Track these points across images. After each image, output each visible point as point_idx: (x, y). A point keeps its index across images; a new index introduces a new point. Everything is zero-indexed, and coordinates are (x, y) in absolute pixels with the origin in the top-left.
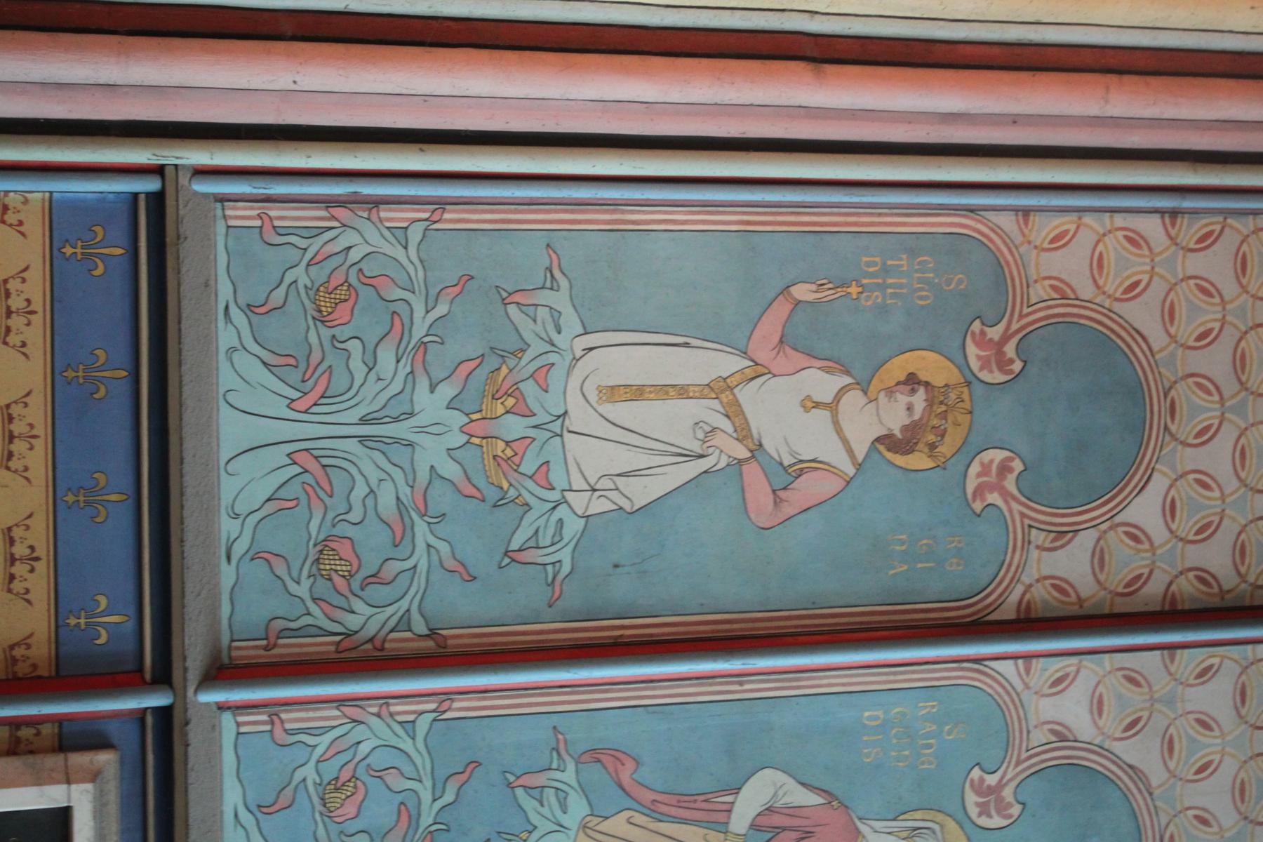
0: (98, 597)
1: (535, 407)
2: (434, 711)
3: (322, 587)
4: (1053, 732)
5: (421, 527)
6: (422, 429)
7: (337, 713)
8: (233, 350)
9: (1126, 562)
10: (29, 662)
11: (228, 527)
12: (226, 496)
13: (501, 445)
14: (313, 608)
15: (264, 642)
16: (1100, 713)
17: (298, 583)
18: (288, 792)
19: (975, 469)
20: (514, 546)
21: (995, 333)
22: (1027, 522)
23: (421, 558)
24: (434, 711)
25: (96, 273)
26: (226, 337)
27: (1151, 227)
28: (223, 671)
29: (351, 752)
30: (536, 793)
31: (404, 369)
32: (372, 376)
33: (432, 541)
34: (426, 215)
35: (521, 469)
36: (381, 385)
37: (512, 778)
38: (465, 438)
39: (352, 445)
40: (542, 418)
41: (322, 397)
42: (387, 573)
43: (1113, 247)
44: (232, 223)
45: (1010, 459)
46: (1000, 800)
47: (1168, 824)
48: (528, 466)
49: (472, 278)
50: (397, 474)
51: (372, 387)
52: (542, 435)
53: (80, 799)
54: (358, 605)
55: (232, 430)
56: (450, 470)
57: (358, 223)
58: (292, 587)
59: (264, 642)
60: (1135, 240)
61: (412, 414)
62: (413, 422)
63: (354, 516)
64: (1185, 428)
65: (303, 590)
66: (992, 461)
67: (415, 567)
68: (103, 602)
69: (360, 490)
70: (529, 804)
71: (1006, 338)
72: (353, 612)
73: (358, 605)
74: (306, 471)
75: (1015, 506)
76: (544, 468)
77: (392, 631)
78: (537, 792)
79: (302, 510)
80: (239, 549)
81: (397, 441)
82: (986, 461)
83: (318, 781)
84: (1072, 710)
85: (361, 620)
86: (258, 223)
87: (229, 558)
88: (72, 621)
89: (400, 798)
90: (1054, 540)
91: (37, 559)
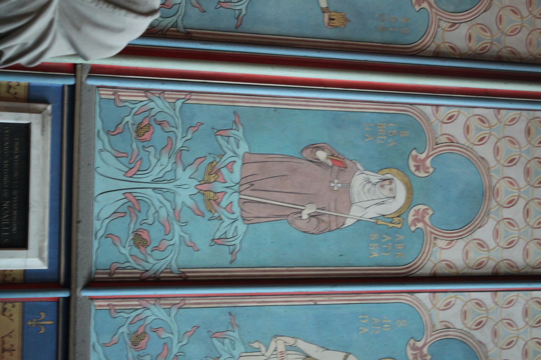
1: (228, 180)
2: (183, 99)
4: (449, 139)
5: (177, 227)
6: (179, 186)
8: (101, 151)
9: (476, 256)
10: (12, 277)
11: (97, 224)
12: (96, 211)
14: (131, 260)
15: (109, 271)
16: (465, 318)
17: (124, 247)
18: (121, 126)
19: (412, 212)
20: (217, 236)
21: (423, 156)
22: (439, 17)
23: (176, 239)
24: (183, 99)
25: (42, 332)
26: (99, 145)
27: (489, 114)
28: (93, 283)
29: (148, 112)
31: (173, 160)
32: (159, 164)
33: (182, 234)
34: (183, 97)
36: (163, 167)
38: (197, 191)
39: (150, 192)
41: (139, 171)
42: (162, 247)
43: (474, 123)
44: (103, 97)
47: (496, 184)
48: (224, 203)
49: (198, 327)
50: (168, 204)
51: (158, 169)
52: (229, 191)
53: (32, 119)
57: (152, 307)
59: (109, 271)
60: (482, 120)
61: (175, 180)
62: (175, 183)
63: (150, 221)
64: (503, 199)
65: (125, 251)
66: (419, 209)
69: (152, 210)
71: (425, 224)
72: (147, 262)
73: (150, 260)
76: (230, 205)
78: (222, 339)
79: (127, 218)
80: (100, 234)
81: (168, 190)
84: (453, 317)
85: (151, 265)
86: (113, 97)
87: (96, 237)
88: (30, 323)
89: (163, 341)
90: (450, 27)
91: (13, 350)
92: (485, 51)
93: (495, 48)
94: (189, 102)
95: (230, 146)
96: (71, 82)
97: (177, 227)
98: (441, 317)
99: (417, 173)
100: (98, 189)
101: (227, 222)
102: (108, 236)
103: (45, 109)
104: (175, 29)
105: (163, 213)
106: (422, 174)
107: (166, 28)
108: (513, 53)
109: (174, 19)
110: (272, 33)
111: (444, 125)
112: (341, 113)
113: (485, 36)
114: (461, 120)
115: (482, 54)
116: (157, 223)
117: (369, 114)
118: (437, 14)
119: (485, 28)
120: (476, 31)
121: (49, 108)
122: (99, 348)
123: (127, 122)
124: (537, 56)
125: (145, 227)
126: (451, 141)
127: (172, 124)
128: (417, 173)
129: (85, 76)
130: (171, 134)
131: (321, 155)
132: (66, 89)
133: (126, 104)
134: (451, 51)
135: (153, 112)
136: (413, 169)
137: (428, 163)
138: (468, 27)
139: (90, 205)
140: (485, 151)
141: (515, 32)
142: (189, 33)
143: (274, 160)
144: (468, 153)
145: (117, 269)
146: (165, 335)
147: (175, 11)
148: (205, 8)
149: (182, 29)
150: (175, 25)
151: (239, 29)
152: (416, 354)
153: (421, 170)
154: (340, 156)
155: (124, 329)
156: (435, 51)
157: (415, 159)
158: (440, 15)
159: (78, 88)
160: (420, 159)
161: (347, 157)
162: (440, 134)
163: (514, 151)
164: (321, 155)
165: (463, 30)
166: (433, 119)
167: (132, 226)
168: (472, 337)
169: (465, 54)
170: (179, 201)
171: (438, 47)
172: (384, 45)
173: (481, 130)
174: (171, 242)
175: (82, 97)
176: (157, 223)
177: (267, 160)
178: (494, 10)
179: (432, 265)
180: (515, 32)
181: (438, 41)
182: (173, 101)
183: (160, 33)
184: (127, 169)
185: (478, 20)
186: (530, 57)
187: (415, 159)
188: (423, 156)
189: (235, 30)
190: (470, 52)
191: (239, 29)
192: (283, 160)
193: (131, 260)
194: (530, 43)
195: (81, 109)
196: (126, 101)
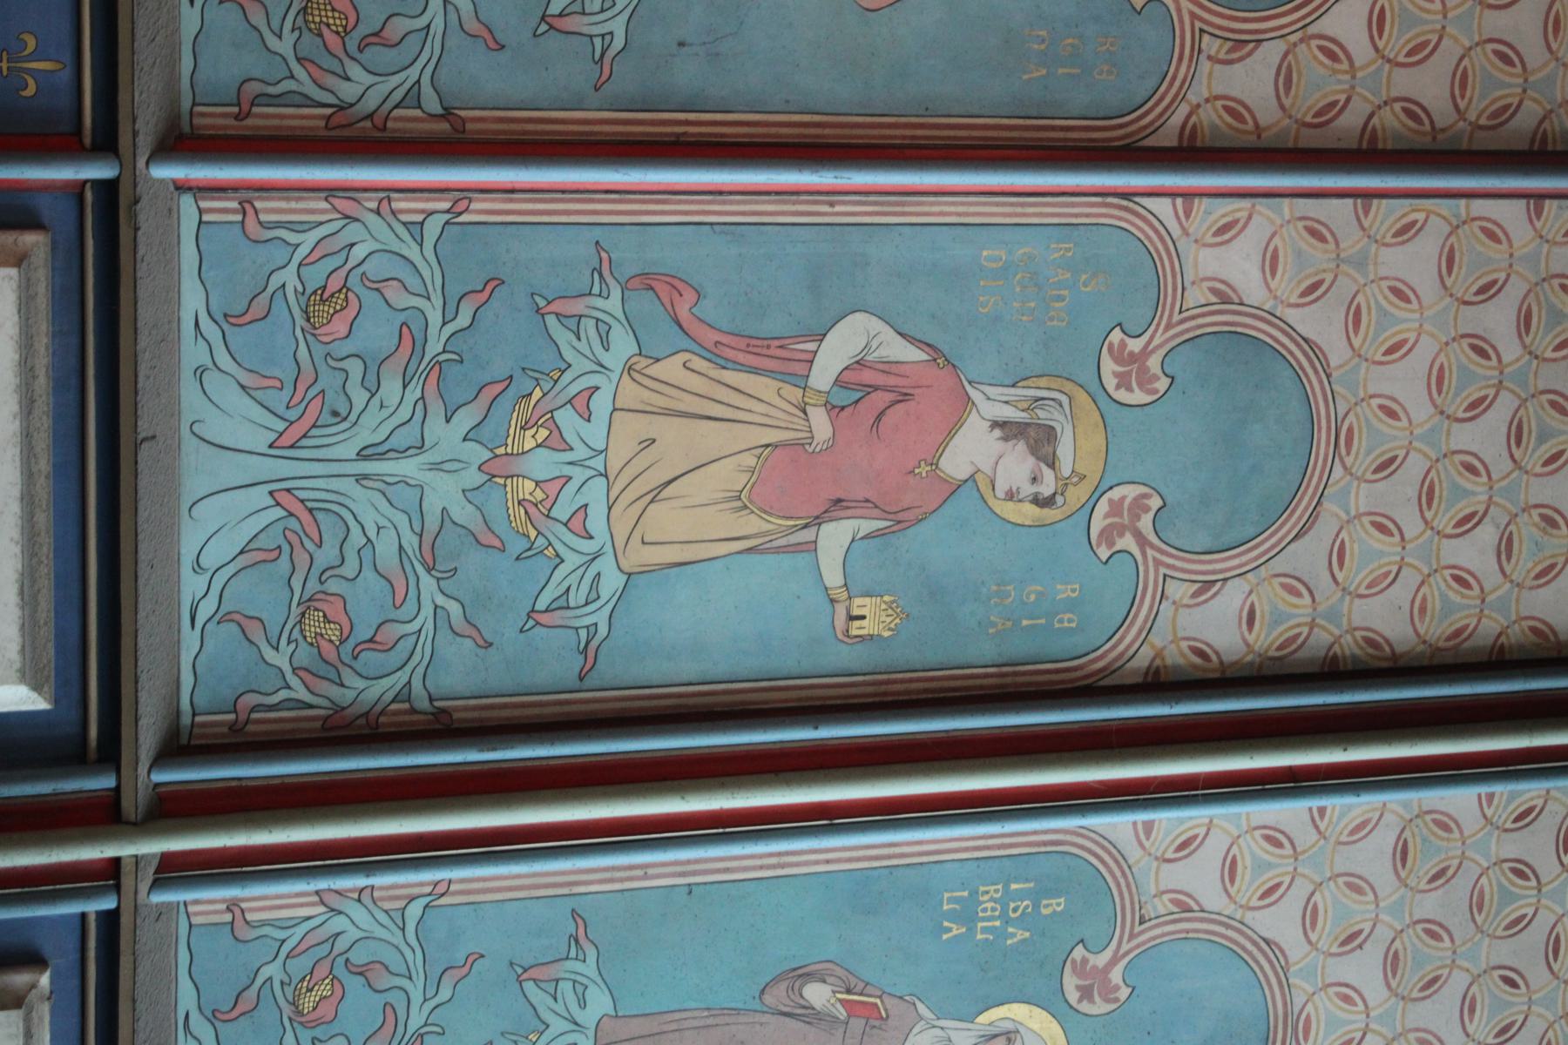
0: (26, 37)
3: (309, 43)
4: (1213, 291)
7: (324, 205)
8: (199, 372)
9: (1318, 84)
11: (192, 585)
13: (529, 485)
14: (294, 681)
21: (1101, 960)
22: (1163, 570)
26: (192, 353)
29: (327, 946)
30: (572, 323)
32: (376, 401)
35: (553, 514)
36: (385, 413)
37: (542, 303)
40: (580, 453)
45: (1145, 496)
46: (1143, 370)
48: (562, 511)
52: (579, 474)
54: (355, 71)
55: (199, 470)
56: (462, 512)
58: (272, 41)
63: (349, 569)
65: (285, 46)
66: (1123, 498)
67: (428, 26)
68: (31, 44)
70: (563, 337)
73: (355, 71)
74: (291, 514)
75: (1125, 947)
76: (581, 514)
77: (396, 107)
78: (574, 323)
80: (200, 619)
82: (1077, 995)
83: (300, 289)
89: (402, 317)
90: (1195, 595)
92: (1294, 647)
93: (1321, 640)
94: (443, 901)
95: (582, 346)
96: (108, 904)
97: (427, 581)
98: (1207, 262)
99: (1085, 1007)
100: (194, 484)
101: (572, 560)
102: (223, 617)
103: (33, 986)
104: (406, 706)
105: (386, 549)
106: (1099, 1007)
107: (379, 708)
108: (1370, 642)
109: (401, 678)
110: (685, 678)
111: (1166, 866)
112: (875, 873)
113: (1296, 606)
114: (1211, 854)
115: (1285, 656)
116: (368, 573)
117: (957, 865)
118: (1158, 563)
119: (1295, 585)
120: (1270, 598)
121: (45, 980)
122: (200, 1025)
123: (270, 978)
124: (1441, 644)
125: (333, 586)
126: (1184, 906)
127: (413, 282)
128: (1085, 1007)
129: (144, 887)
130: (392, 997)
131: (817, 994)
132: (92, 920)
133: (267, 930)
134: (1197, 660)
135: (359, 252)
136: (1073, 996)
137: (1116, 976)
138: (1247, 588)
139: (171, 532)
140: (1281, 923)
141: (1383, 582)
142: (443, 711)
143: (687, 1024)
144: (1230, 933)
145: (253, 710)
146: (385, 981)
147: (405, 655)
148: (489, 638)
149: (423, 704)
150: (404, 695)
151: (588, 683)
152: (1129, 373)
153: (1097, 998)
154: (869, 990)
155: (289, 276)
156: (1149, 668)
157: (1081, 969)
158: (1169, 566)
159: (125, 920)
160: (1094, 967)
161: (888, 990)
162: (1153, 892)
163: (1360, 911)
164: (817, 994)
165: (1232, 598)
166: (1134, 854)
167: (297, 584)
168: (1289, 330)
169: (1236, 663)
170: (433, 505)
171: (1159, 654)
172: (1005, 669)
173: (1270, 866)
174: (409, 628)
175: (138, 942)
176: (368, 573)
177: (665, 1028)
178: (1324, 530)
179: (1151, 654)
180: (1383, 582)
181: (1157, 640)
182: (419, 218)
183: (362, 721)
184: (281, 426)
185: (1278, 565)
186: (1421, 648)
187: (1081, 969)
188: (1101, 960)
189: (577, 685)
190: (1249, 658)
191: (588, 683)
192: (710, 1021)
193: (294, 681)
194: (1423, 610)
195: (136, 976)
196: (264, 923)
